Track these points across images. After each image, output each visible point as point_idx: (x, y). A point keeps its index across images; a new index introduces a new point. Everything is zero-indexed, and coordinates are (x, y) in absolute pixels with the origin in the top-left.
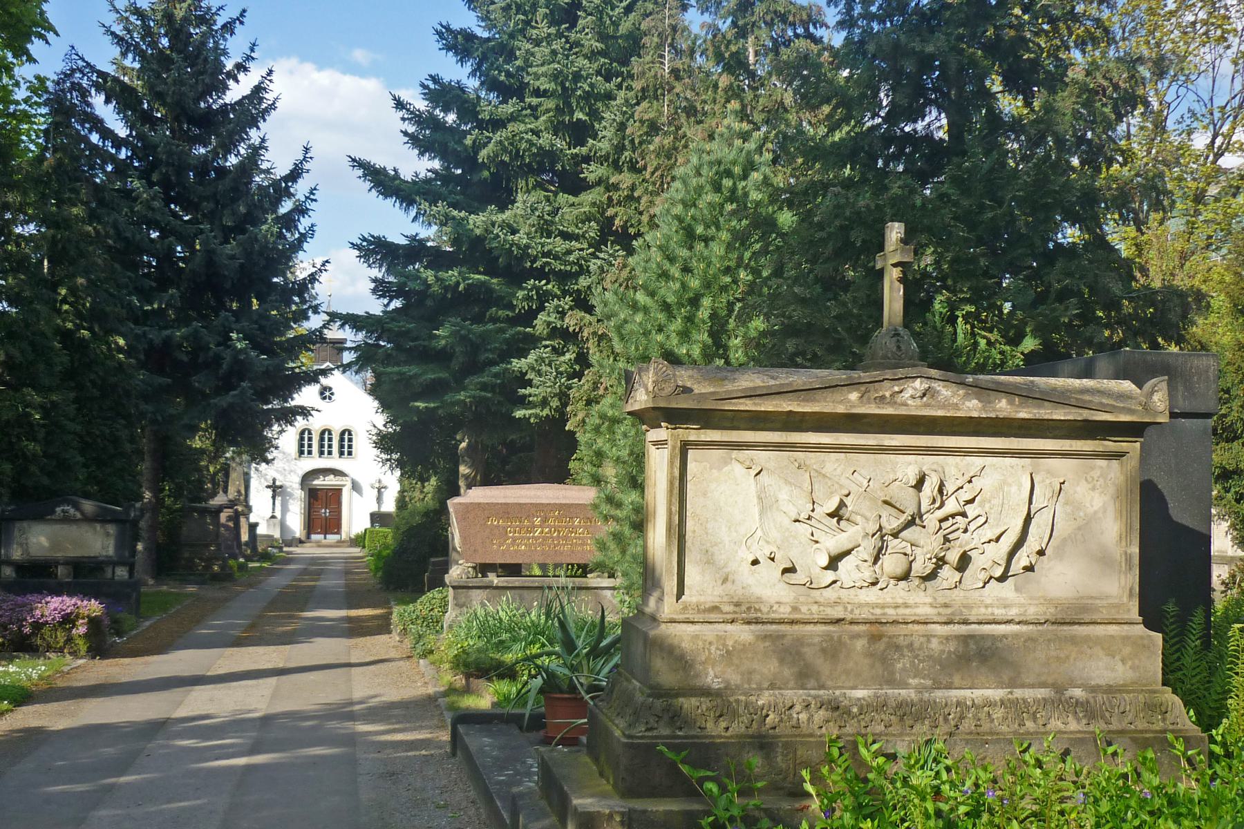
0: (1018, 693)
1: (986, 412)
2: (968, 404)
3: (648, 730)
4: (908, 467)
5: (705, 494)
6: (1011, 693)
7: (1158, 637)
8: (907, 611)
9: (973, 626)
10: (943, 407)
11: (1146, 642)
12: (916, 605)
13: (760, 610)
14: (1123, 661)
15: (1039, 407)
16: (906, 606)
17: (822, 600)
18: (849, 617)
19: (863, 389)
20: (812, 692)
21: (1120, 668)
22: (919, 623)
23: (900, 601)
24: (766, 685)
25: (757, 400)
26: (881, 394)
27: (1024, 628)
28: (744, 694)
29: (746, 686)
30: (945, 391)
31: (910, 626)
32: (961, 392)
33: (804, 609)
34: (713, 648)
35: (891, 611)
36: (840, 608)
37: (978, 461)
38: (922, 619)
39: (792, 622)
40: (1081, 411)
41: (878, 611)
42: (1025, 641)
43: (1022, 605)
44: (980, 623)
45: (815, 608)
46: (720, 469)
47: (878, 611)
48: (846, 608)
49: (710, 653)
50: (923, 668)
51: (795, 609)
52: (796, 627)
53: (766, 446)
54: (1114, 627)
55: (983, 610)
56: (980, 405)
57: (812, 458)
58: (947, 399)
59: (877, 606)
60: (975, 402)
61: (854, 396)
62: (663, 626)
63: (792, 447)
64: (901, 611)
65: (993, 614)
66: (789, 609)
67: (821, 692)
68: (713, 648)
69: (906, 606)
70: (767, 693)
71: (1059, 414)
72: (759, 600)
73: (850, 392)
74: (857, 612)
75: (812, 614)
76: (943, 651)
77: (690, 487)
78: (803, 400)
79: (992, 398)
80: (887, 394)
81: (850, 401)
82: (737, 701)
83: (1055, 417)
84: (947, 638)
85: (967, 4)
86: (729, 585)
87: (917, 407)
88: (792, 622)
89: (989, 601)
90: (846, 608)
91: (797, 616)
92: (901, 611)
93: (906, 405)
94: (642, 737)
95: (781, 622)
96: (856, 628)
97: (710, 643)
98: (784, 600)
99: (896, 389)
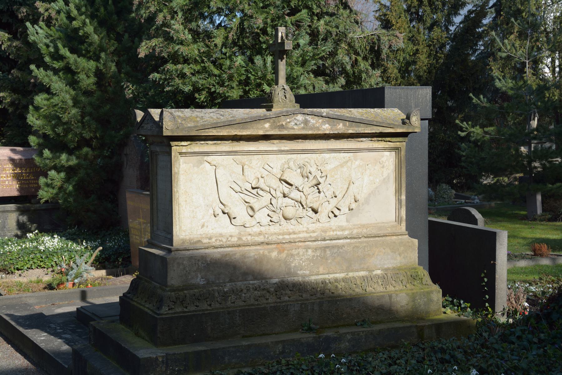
0: (351, 274)
1: (332, 130)
2: (324, 127)
3: (169, 309)
4: (277, 162)
5: (191, 181)
6: (347, 275)
7: (416, 241)
8: (295, 236)
9: (328, 242)
10: (311, 129)
11: (410, 244)
12: (300, 232)
13: (222, 241)
14: (400, 254)
15: (359, 127)
16: (294, 233)
17: (252, 233)
18: (266, 240)
19: (271, 121)
20: (251, 282)
21: (398, 258)
22: (301, 241)
23: (291, 231)
24: (227, 280)
25: (218, 129)
26: (281, 123)
27: (353, 241)
28: (217, 286)
29: (217, 281)
30: (313, 120)
31: (297, 243)
32: (320, 121)
33: (244, 238)
34: (200, 263)
35: (287, 237)
36: (262, 237)
37: (327, 156)
38: (303, 240)
39: (239, 246)
40: (378, 128)
41: (281, 237)
42: (354, 248)
43: (350, 229)
44: (331, 240)
45: (249, 238)
46: (198, 167)
47: (281, 237)
48: (265, 237)
49: (198, 266)
50: (305, 265)
51: (240, 239)
52: (241, 249)
53: (221, 153)
54: (395, 237)
55: (332, 233)
56: (329, 127)
57: (244, 159)
58: (313, 125)
59: (279, 234)
60: (327, 125)
61: (267, 125)
62: (173, 253)
63: (249, 153)
64: (292, 236)
65: (336, 235)
66: (236, 239)
67: (255, 282)
68: (200, 263)
69: (294, 233)
70: (228, 285)
71: (368, 130)
72: (221, 235)
73: (265, 123)
74: (270, 238)
75: (248, 241)
76: (314, 256)
77: (289, 181)
78: (242, 128)
79: (335, 123)
80: (284, 123)
81: (265, 128)
82: (213, 290)
83: (366, 132)
84: (316, 249)
85: (3, 135)
86: (205, 228)
87: (299, 130)
88: (239, 246)
89: (334, 228)
90: (265, 237)
91: (240, 242)
92: (292, 236)
93: (294, 129)
94: (166, 314)
95: (233, 246)
96: (270, 246)
97: (198, 260)
98: (233, 234)
99: (288, 120)
